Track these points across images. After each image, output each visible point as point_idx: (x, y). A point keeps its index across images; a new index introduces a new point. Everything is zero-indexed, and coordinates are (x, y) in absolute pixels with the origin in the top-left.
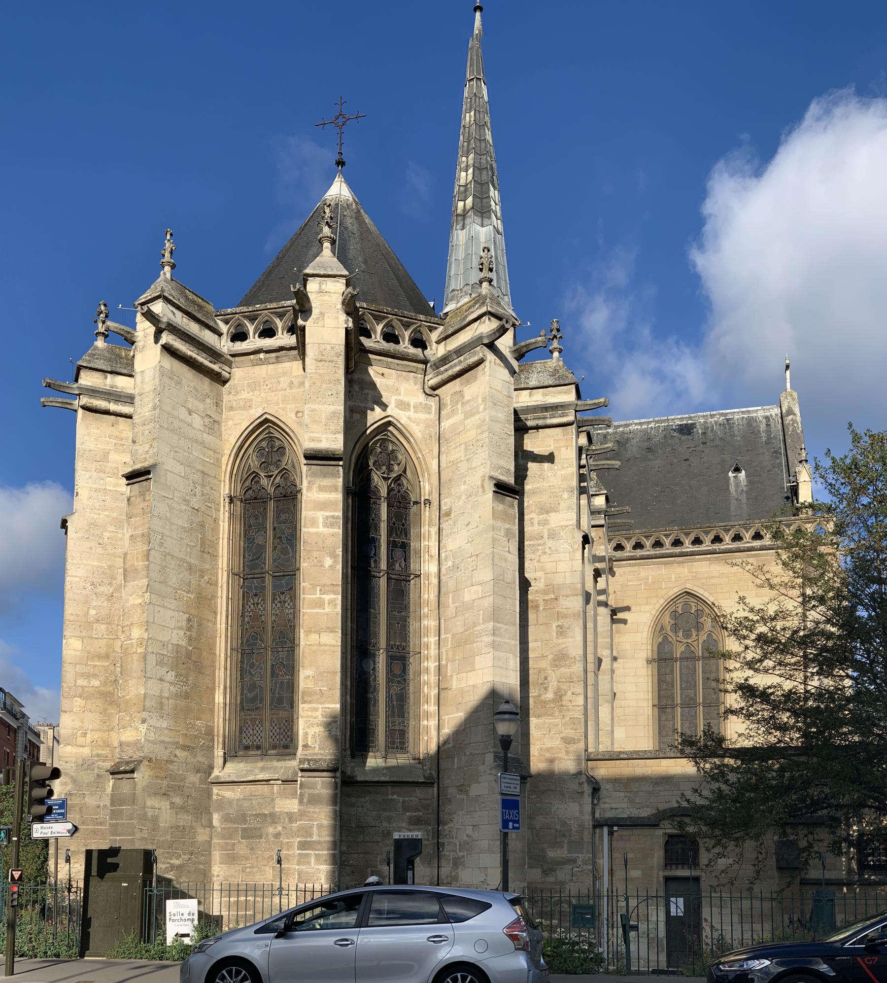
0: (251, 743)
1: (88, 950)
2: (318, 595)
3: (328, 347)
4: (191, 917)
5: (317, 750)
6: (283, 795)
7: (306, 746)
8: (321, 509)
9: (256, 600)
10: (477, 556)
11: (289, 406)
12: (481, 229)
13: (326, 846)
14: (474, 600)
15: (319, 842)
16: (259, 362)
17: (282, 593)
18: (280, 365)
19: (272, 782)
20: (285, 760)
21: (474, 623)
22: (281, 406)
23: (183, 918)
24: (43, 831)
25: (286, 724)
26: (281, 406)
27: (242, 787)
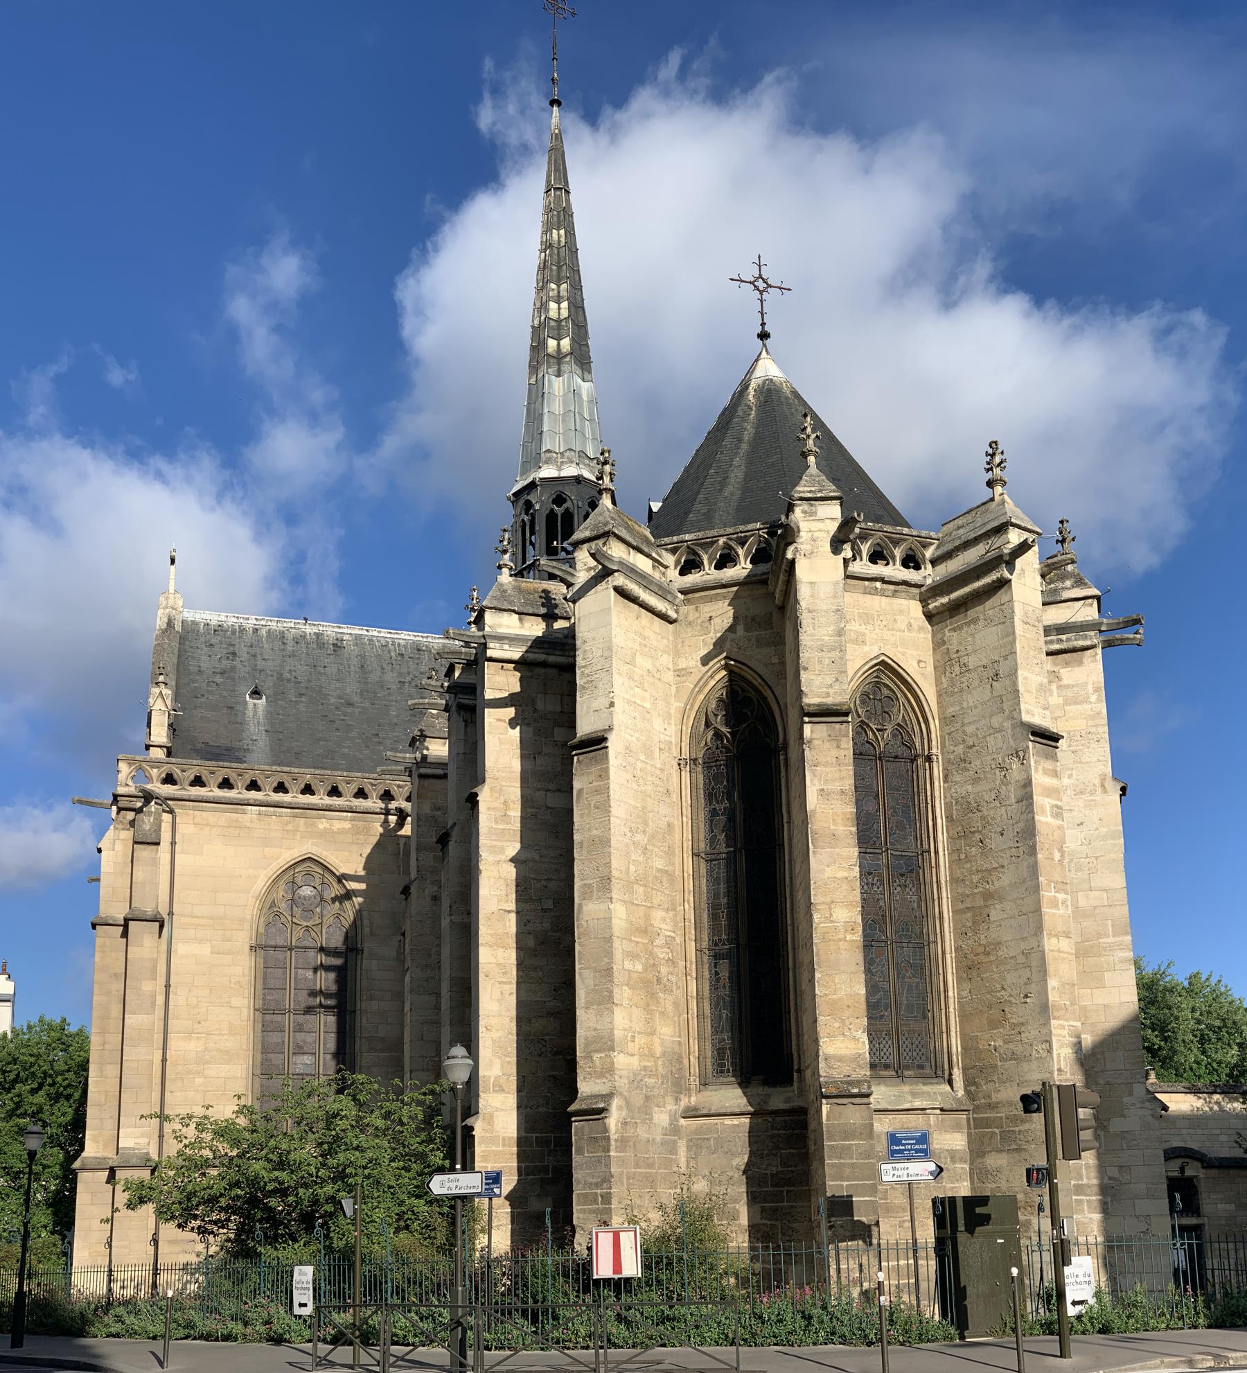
0: (877, 1061)
1: (968, 1329)
2: (1053, 894)
3: (1031, 609)
4: (1087, 1279)
5: (1068, 1076)
6: (942, 1128)
7: (1060, 1070)
8: (1048, 796)
9: (870, 880)
10: (1097, 858)
11: (909, 652)
12: (582, 383)
13: (1095, 1189)
14: (1095, 908)
15: (1088, 1186)
16: (873, 591)
17: (902, 875)
18: (895, 601)
19: (928, 1111)
20: (932, 1084)
21: (1098, 933)
22: (899, 649)
23: (1078, 1280)
24: (896, 1172)
25: (919, 1039)
26: (899, 649)
27: (890, 1117)
